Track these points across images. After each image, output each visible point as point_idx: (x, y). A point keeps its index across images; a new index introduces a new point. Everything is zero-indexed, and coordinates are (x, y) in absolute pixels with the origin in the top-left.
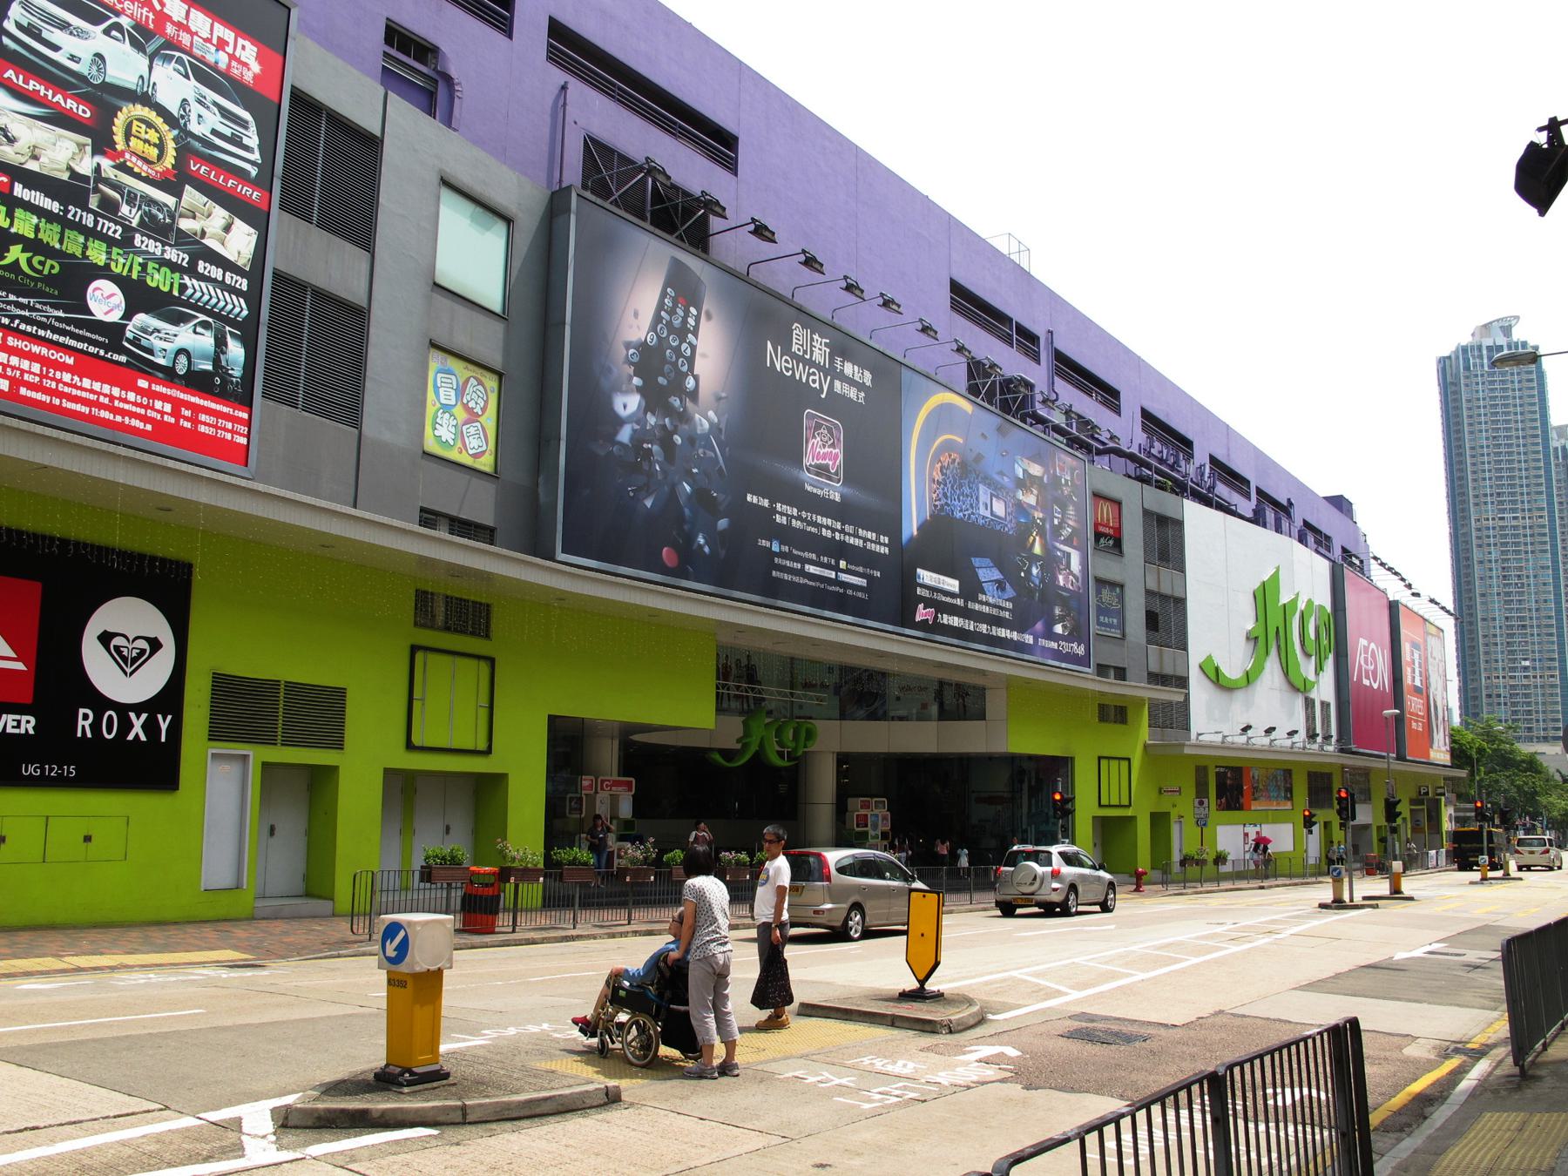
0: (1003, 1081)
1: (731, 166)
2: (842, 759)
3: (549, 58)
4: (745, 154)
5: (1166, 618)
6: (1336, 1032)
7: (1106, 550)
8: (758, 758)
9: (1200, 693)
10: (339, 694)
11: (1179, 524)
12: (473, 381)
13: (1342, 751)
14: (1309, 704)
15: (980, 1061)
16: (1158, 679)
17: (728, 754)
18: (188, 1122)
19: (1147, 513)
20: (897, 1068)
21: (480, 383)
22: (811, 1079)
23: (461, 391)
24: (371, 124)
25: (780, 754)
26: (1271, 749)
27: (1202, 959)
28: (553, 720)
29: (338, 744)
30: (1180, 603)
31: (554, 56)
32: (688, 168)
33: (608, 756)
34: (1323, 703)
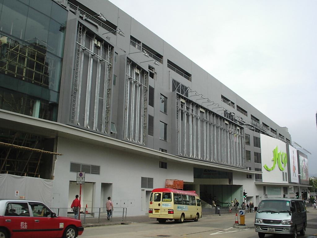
4: (193, 77)
9: (264, 173)
10: (153, 179)
11: (260, 139)
16: (257, 170)
19: (254, 137)
27: (228, 229)
31: (168, 66)
34: (285, 173)
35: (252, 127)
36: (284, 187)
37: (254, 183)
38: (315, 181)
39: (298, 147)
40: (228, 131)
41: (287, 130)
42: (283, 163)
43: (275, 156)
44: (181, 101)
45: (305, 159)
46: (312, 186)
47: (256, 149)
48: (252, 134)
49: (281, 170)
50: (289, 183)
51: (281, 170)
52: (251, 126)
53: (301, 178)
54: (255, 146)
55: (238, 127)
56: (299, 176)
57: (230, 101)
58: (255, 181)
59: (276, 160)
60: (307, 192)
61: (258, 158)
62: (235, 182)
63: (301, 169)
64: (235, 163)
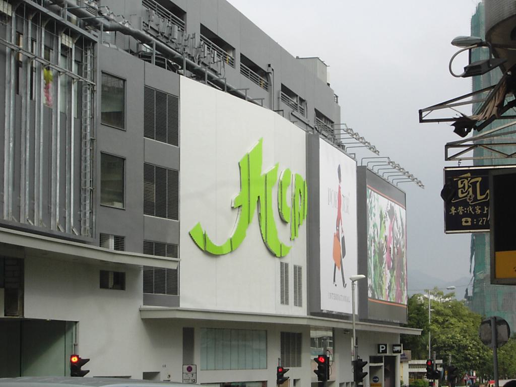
5: (163, 190)
9: (190, 265)
19: (148, 91)
28: (184, 328)
35: (144, 40)
36: (283, 334)
37: (137, 311)
38: (440, 308)
39: (363, 153)
40: (8, 50)
41: (324, 73)
42: (284, 222)
43: (246, 183)
44: (62, 44)
45: (398, 208)
46: (417, 332)
47: (156, 151)
48: (141, 76)
49: (274, 255)
50: (312, 314)
51: (274, 255)
52: (137, 36)
53: (370, 295)
54: (148, 133)
55: (66, 33)
56: (363, 285)
57: (297, 96)
58: (140, 303)
59: (249, 207)
60: (399, 355)
61: (161, 192)
62: (38, 307)
63: (371, 252)
64: (39, 214)
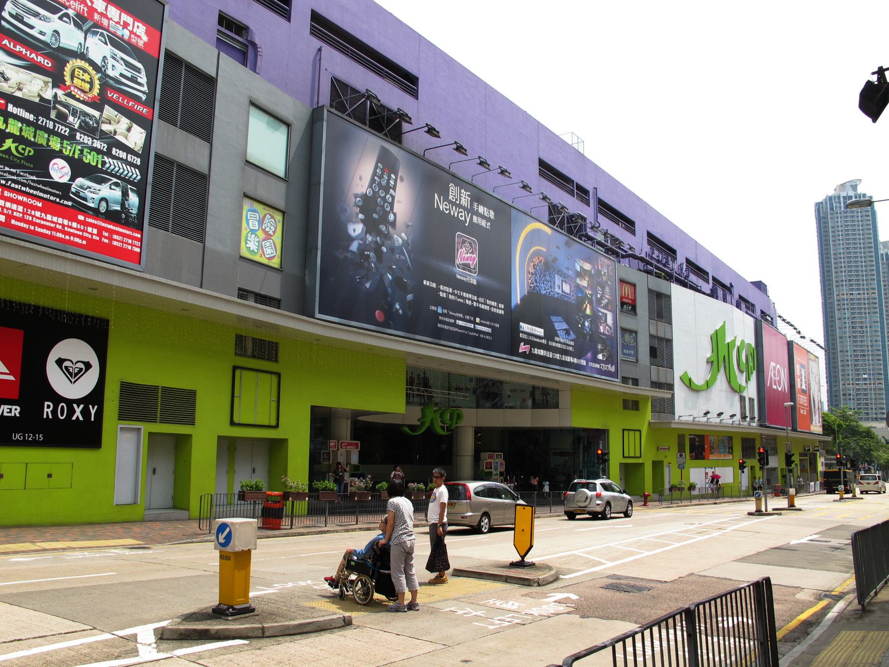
0: (569, 613)
1: (415, 94)
2: (478, 430)
3: (311, 33)
4: (423, 87)
5: (661, 351)
6: (757, 585)
7: (627, 312)
8: (430, 430)
9: (680, 393)
10: (192, 394)
11: (669, 297)
12: (268, 216)
13: (761, 426)
14: (742, 399)
15: (556, 602)
16: (657, 385)
17: (413, 428)
18: (107, 636)
19: (650, 291)
20: (509, 606)
21: (272, 217)
22: (460, 612)
23: (261, 222)
24: (211, 71)
25: (442, 428)
26: (720, 425)
27: (681, 544)
29: (192, 422)
30: (669, 342)
31: (314, 32)
32: (390, 96)
33: (345, 429)
34: (750, 399)
